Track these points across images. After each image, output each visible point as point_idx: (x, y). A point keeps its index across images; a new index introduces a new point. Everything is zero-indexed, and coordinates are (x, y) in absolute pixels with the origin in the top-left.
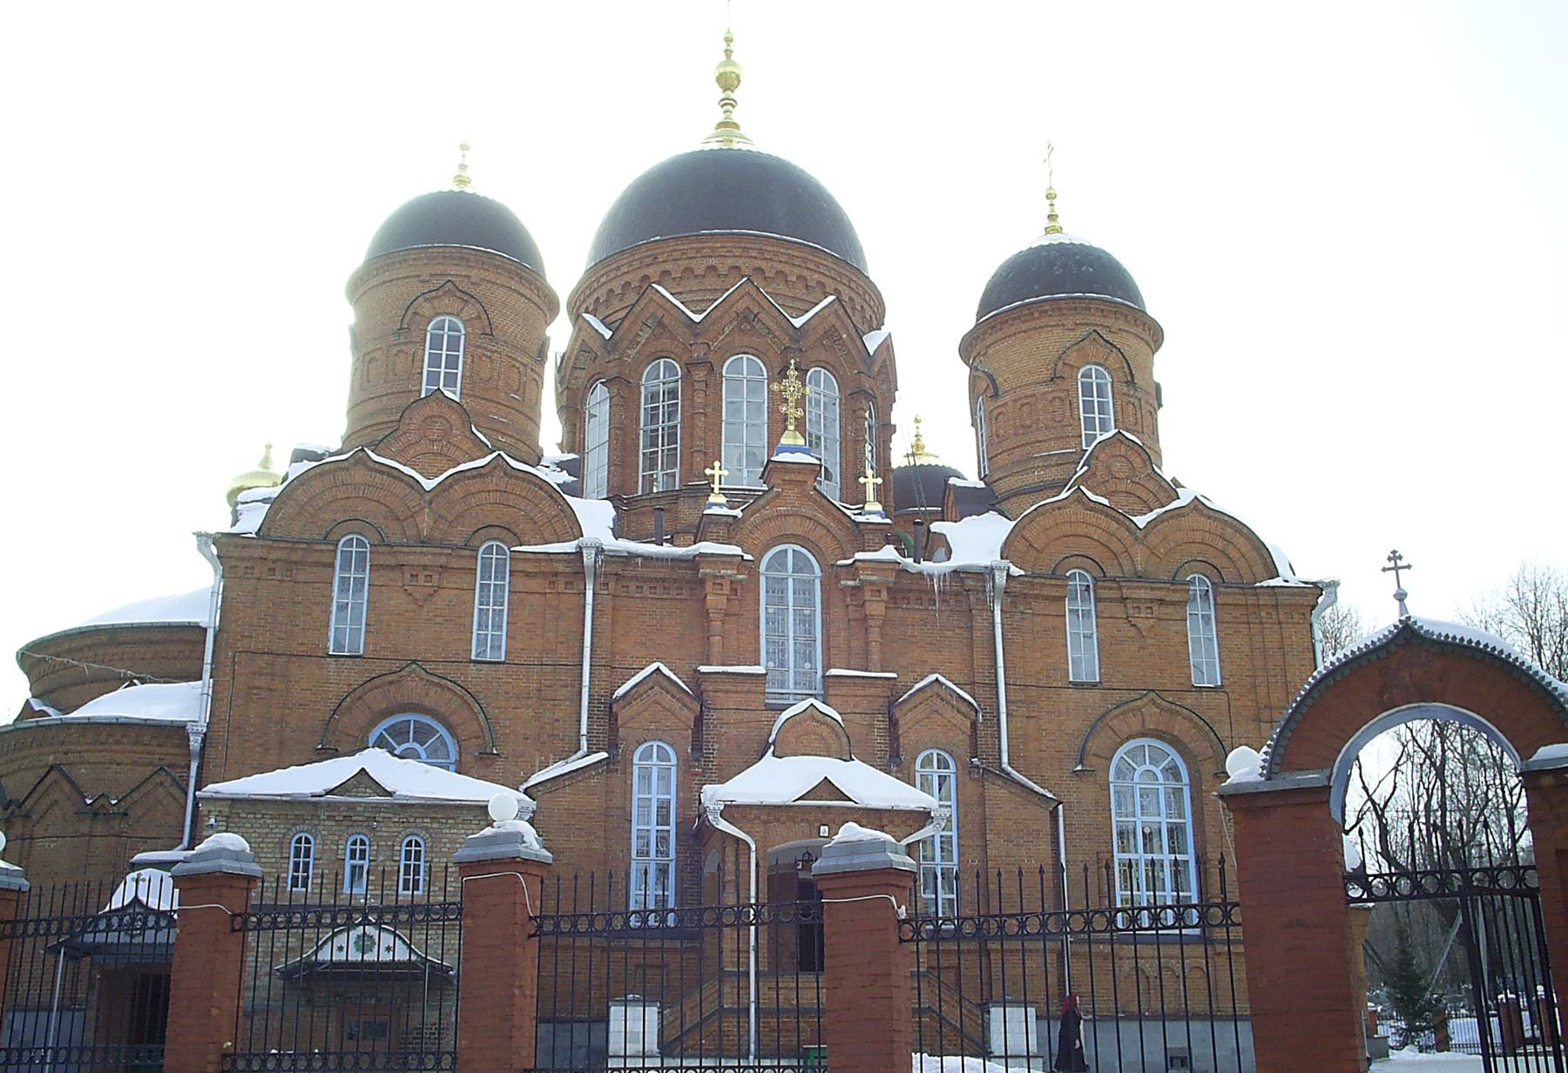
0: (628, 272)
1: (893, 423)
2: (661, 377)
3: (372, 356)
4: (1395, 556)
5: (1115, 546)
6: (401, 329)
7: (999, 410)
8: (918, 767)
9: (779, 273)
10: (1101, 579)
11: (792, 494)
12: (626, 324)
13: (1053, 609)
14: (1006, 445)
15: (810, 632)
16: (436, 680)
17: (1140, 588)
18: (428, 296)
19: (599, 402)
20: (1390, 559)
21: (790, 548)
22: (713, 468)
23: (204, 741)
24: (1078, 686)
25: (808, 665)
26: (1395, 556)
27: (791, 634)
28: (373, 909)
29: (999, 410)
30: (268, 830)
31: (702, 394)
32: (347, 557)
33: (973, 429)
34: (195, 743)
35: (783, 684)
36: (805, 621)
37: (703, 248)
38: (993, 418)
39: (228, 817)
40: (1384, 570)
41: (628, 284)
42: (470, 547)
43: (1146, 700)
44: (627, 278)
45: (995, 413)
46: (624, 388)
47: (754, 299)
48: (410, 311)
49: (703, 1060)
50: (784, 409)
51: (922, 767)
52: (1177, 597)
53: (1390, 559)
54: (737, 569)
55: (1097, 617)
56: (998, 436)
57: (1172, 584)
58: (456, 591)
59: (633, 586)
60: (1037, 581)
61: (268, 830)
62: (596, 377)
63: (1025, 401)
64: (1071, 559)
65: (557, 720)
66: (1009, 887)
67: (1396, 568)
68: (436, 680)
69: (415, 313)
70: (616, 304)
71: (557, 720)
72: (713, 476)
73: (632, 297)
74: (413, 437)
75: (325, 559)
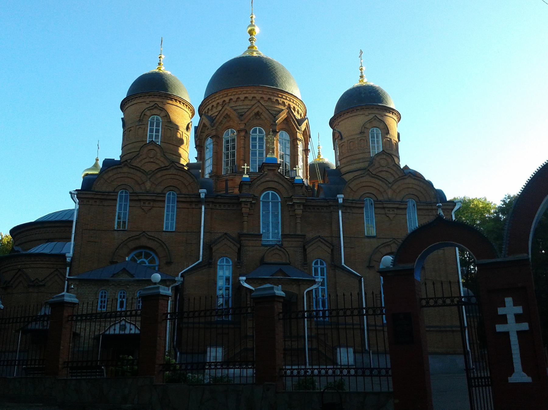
0: (218, 99)
1: (309, 149)
2: (230, 135)
3: (130, 129)
5: (381, 189)
6: (140, 120)
7: (343, 144)
9: (269, 99)
10: (377, 201)
11: (271, 174)
12: (218, 117)
14: (345, 156)
15: (278, 219)
16: (152, 238)
17: (390, 204)
18: (149, 108)
19: (209, 143)
21: (270, 192)
22: (244, 166)
23: (72, 259)
24: (369, 237)
25: (276, 231)
27: (271, 221)
30: (91, 289)
31: (243, 141)
32: (121, 197)
33: (334, 151)
34: (68, 260)
35: (268, 237)
36: (275, 216)
37: (244, 90)
38: (341, 147)
39: (78, 285)
41: (218, 103)
42: (163, 194)
43: (392, 242)
44: (218, 101)
45: (341, 145)
46: (217, 138)
47: (261, 108)
48: (143, 114)
49: (313, 366)
50: (268, 145)
51: (314, 265)
52: (403, 206)
54: (253, 199)
55: (375, 214)
56: (342, 153)
57: (401, 202)
58: (159, 208)
59: (218, 205)
60: (354, 202)
61: (91, 289)
62: (208, 135)
63: (351, 141)
64: (366, 194)
65: (192, 251)
68: (152, 238)
69: (145, 114)
70: (214, 110)
71: (192, 251)
72: (244, 168)
73: (220, 108)
74: (144, 156)
75: (114, 197)
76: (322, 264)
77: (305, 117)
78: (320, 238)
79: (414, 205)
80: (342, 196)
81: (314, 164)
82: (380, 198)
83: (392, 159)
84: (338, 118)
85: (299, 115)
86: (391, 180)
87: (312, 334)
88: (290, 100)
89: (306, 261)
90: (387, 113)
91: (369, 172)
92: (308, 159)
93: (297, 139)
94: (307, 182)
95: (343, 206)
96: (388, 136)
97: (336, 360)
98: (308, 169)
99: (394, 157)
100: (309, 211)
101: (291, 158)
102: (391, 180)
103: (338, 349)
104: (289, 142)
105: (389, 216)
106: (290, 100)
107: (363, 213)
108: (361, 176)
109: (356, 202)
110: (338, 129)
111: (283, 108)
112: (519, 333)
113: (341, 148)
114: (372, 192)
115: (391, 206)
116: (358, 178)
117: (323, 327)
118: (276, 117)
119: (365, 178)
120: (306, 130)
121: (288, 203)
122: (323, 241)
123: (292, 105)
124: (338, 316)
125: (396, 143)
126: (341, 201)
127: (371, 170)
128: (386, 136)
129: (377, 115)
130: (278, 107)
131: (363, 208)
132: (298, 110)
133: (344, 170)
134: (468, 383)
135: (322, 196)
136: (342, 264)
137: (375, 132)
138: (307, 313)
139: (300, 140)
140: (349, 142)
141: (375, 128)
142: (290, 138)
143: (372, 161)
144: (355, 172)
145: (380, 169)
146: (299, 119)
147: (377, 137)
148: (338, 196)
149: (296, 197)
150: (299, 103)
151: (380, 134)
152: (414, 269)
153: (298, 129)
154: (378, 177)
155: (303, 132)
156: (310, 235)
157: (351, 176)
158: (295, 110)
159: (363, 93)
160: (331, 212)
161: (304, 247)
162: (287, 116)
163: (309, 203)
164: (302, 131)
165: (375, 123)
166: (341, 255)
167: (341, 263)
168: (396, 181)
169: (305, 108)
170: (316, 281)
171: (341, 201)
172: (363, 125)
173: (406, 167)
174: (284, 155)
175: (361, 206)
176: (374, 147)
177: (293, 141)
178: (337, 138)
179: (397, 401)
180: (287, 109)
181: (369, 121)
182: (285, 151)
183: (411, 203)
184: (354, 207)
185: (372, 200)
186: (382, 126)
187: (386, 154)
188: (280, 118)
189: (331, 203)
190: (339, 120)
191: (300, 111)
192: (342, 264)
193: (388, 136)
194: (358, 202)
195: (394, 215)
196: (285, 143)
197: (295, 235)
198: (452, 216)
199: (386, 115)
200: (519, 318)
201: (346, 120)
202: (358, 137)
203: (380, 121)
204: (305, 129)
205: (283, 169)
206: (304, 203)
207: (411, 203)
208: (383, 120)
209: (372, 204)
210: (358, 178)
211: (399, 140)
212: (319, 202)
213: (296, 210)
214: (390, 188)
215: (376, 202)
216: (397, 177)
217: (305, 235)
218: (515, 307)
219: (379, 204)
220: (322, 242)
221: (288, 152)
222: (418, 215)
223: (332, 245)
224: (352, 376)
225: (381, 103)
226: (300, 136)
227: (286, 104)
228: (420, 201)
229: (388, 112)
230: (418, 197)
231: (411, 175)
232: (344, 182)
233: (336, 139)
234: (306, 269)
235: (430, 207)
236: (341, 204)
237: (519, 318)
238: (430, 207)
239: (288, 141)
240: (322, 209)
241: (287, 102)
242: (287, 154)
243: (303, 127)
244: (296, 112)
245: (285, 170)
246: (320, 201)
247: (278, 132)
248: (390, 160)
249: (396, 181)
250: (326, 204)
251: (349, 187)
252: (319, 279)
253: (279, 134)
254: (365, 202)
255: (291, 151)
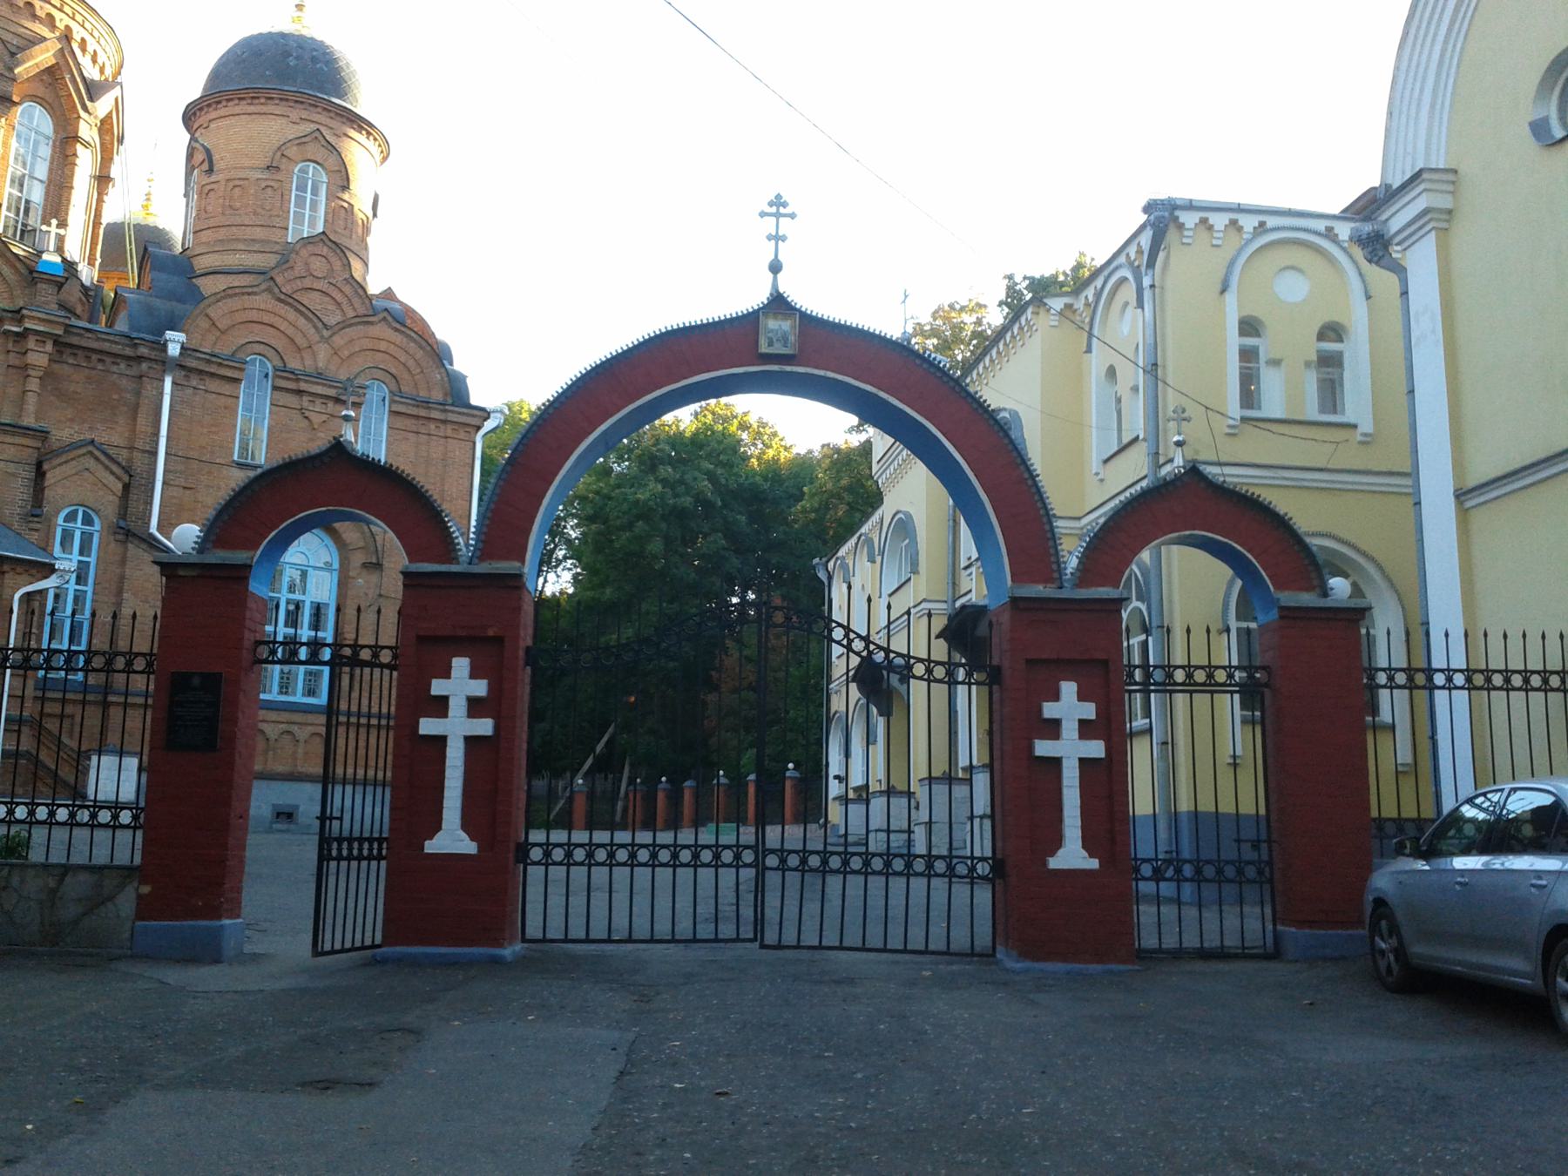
4: (778, 202)
5: (300, 340)
8: (60, 520)
10: (283, 371)
13: (227, 388)
14: (212, 223)
17: (318, 384)
20: (771, 204)
22: (49, 225)
26: (778, 202)
28: (364, 664)
29: (212, 186)
33: (185, 199)
38: (205, 193)
40: (763, 214)
45: (209, 187)
51: (65, 521)
53: (771, 204)
55: (272, 404)
60: (214, 359)
63: (237, 183)
64: (254, 345)
66: (1496, 643)
67: (778, 215)
76: (88, 521)
77: (115, 77)
78: (95, 446)
79: (384, 400)
80: (181, 337)
81: (123, 223)
82: (294, 364)
83: (345, 262)
84: (211, 109)
85: (97, 67)
86: (333, 319)
87: (24, 713)
88: (74, 14)
89: (40, 507)
90: (352, 130)
91: (272, 283)
92: (105, 205)
93: (76, 138)
94: (88, 274)
95: (179, 365)
96: (346, 196)
97: (85, 786)
98: (98, 238)
99: (349, 254)
100: (71, 361)
101: (47, 194)
102: (333, 319)
103: (95, 759)
104: (51, 143)
105: (311, 418)
106: (74, 14)
107: (238, 398)
108: (250, 290)
109: (219, 361)
110: (205, 139)
111: (43, 31)
112: (471, 741)
113: (204, 196)
114: (273, 342)
115: (319, 390)
116: (236, 295)
117: (60, 695)
118: (18, 56)
119: (257, 297)
120: (111, 118)
121: (7, 327)
122: (102, 458)
123: (78, 32)
124: (108, 669)
125: (365, 219)
126: (174, 350)
127: (279, 280)
128: (340, 195)
129: (323, 129)
130: (29, 25)
131: (237, 381)
132: (95, 51)
133: (202, 263)
134: (321, 849)
135: (122, 325)
136: (151, 531)
137: (310, 175)
138: (77, 663)
139: (86, 145)
140: (231, 184)
141: (312, 165)
142: (56, 131)
143: (286, 255)
144: (234, 276)
145: (308, 283)
146: (92, 80)
147: (315, 192)
148: (169, 334)
149: (34, 314)
150: (103, 33)
151: (325, 185)
152: (250, 566)
153: (85, 109)
154: (296, 304)
155: (102, 122)
156: (63, 434)
157: (221, 283)
158: (84, 50)
159: (294, 54)
160: (141, 377)
161: (39, 465)
162: (54, 61)
163: (75, 340)
164: (96, 117)
165: (313, 150)
166: (151, 504)
167: (149, 527)
168: (344, 325)
169: (120, 50)
170: (56, 567)
171: (174, 350)
172: (279, 148)
173: (388, 294)
174: (27, 177)
175: (235, 375)
176: (299, 218)
177: (61, 142)
178: (200, 161)
179: (145, 889)
180: (59, 39)
181: (297, 141)
182: (33, 165)
183: (377, 394)
184: (213, 375)
185: (269, 365)
186: (332, 161)
187: (330, 244)
188: (29, 60)
189: (143, 351)
190: (213, 115)
191: (101, 58)
192: (151, 531)
193: (346, 196)
194: (226, 363)
195: (324, 417)
196: (36, 143)
197: (14, 426)
198: (474, 443)
199: (350, 134)
200: (475, 707)
201: (233, 120)
202: (260, 176)
203: (330, 148)
204: (109, 116)
205: (17, 222)
206: (60, 336)
207: (377, 394)
208: (337, 146)
209: (266, 376)
210: (236, 295)
211: (375, 215)
212: (108, 341)
213: (30, 354)
214: (327, 340)
215: (278, 373)
216: (351, 314)
217: (48, 432)
218: (473, 682)
219: (288, 379)
220: (97, 459)
221: (42, 171)
222: (390, 428)
223: (127, 472)
224: (79, 825)
225: (340, 98)
226: (87, 130)
227: (58, 24)
228: (400, 392)
229: (354, 129)
230: (397, 381)
231: (390, 319)
232: (196, 296)
233: (193, 168)
234: (36, 530)
235: (423, 413)
236: (173, 358)
237: (475, 707)
238: (423, 413)
239: (48, 138)
240: (113, 363)
241: (61, 20)
242: (36, 175)
243: (103, 106)
244: (88, 57)
245: (23, 225)
246: (112, 338)
247: (15, 104)
248: (337, 265)
249: (344, 325)
250: (128, 352)
251: (207, 315)
252: (67, 562)
253: (20, 109)
254: (249, 367)
255: (51, 170)
